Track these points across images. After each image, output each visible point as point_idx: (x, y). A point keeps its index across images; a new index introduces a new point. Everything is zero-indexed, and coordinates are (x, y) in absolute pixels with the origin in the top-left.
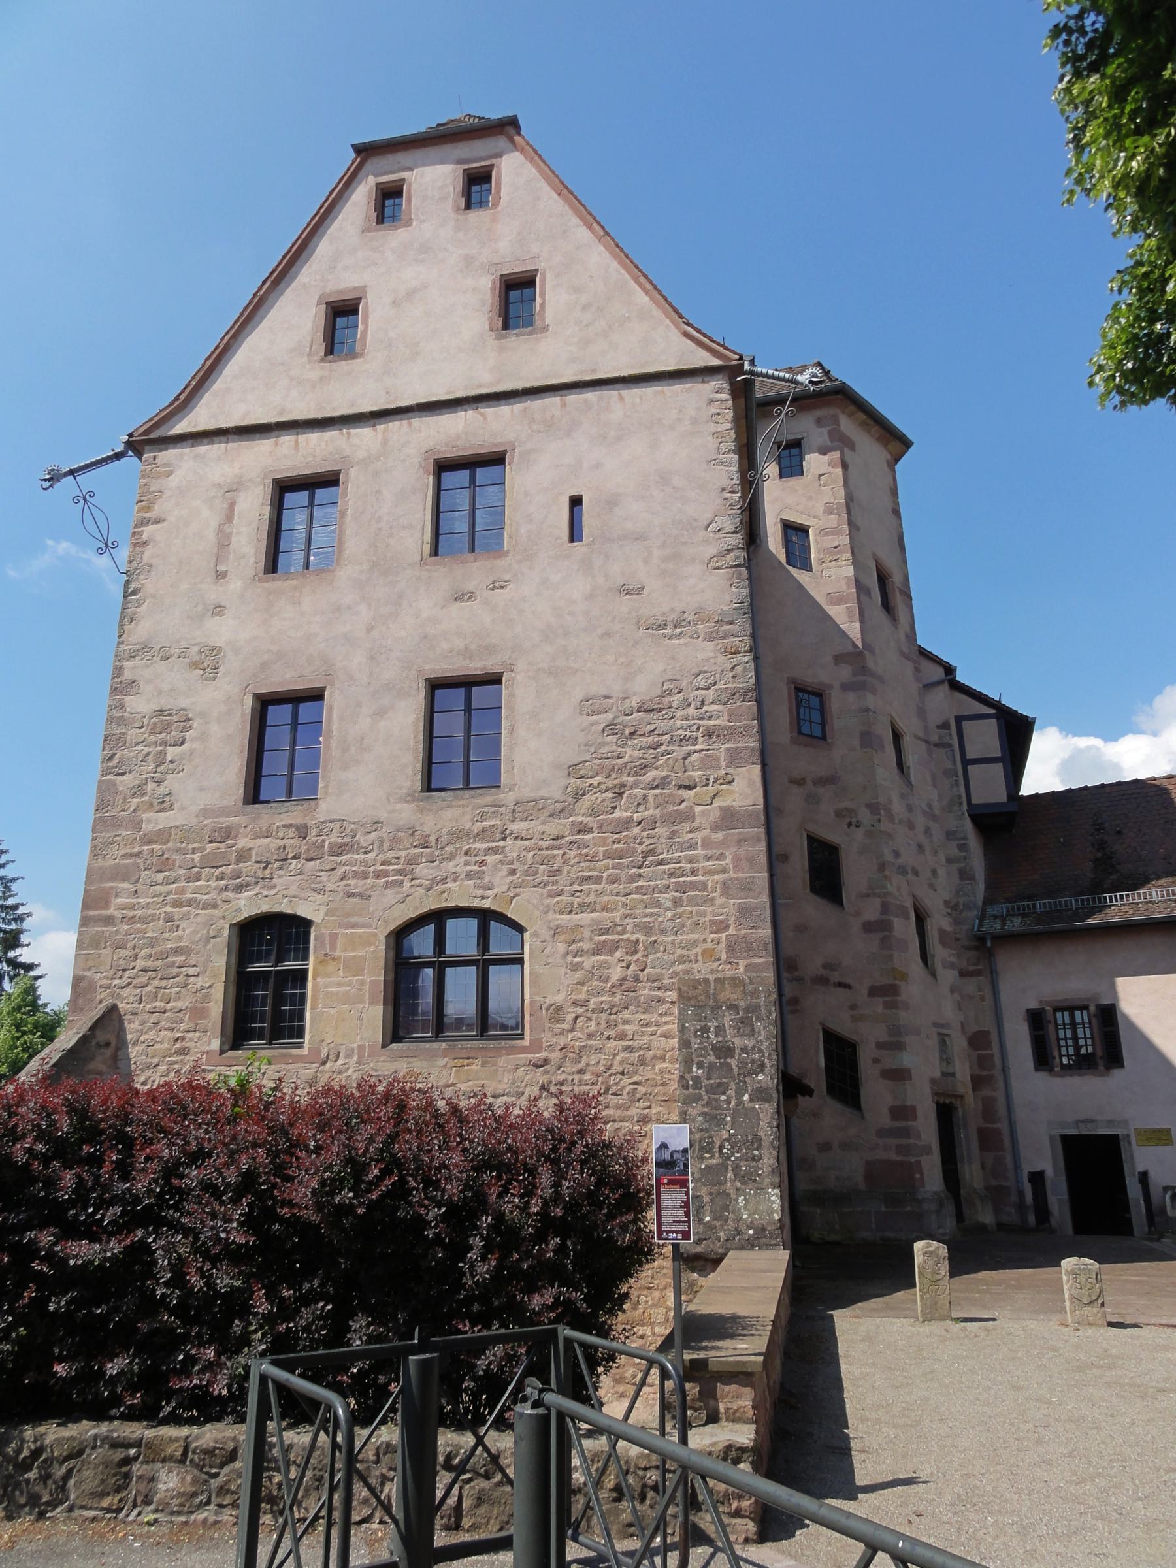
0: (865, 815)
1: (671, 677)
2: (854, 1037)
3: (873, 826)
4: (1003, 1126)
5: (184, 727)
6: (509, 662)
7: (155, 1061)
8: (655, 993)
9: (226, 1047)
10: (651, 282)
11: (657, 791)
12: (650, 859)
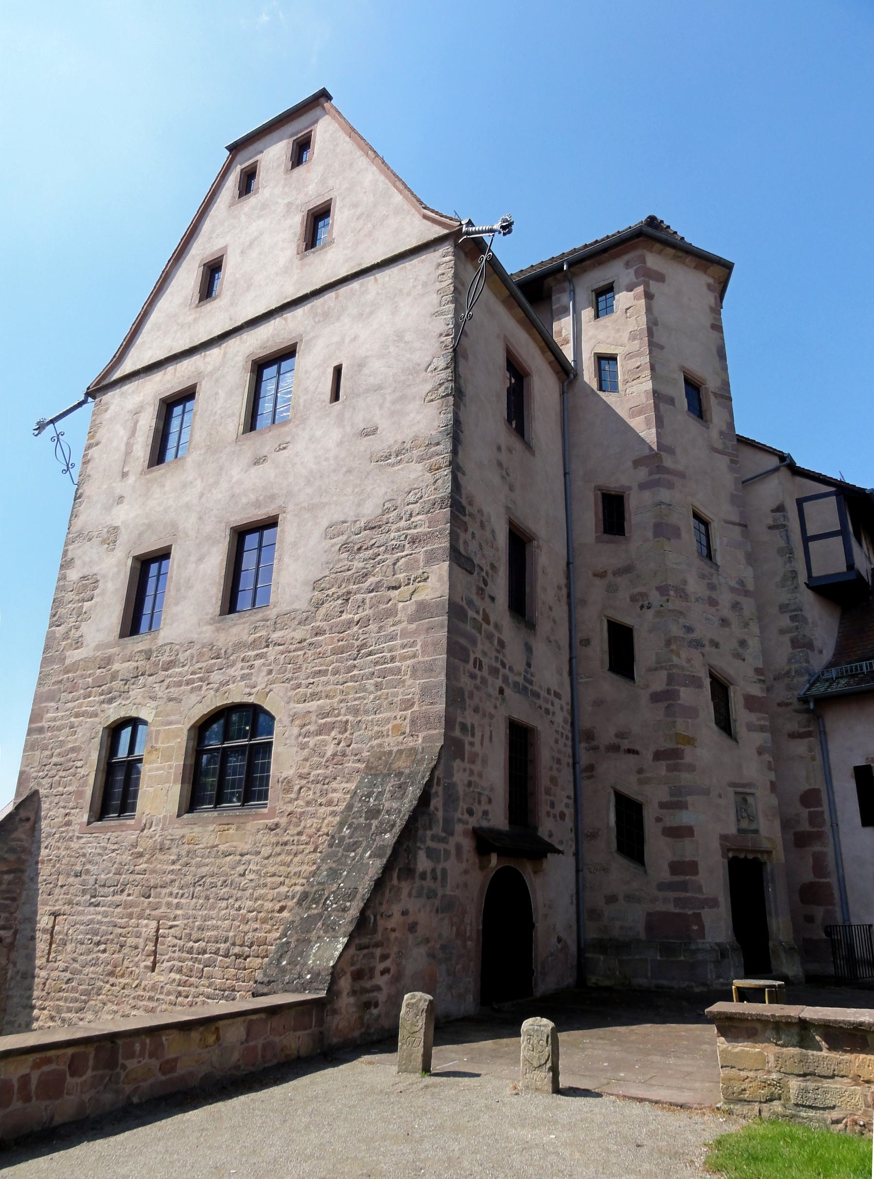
0: (655, 597)
1: (390, 498)
2: (640, 798)
3: (662, 606)
4: (833, 880)
5: (94, 587)
6: (283, 505)
7: (54, 830)
8: (356, 765)
9: (93, 819)
10: (403, 183)
11: (373, 594)
12: (362, 651)
